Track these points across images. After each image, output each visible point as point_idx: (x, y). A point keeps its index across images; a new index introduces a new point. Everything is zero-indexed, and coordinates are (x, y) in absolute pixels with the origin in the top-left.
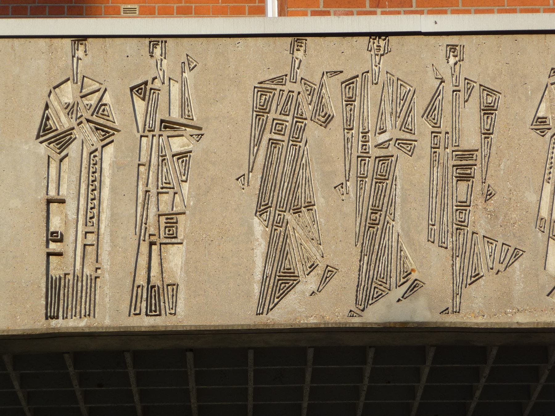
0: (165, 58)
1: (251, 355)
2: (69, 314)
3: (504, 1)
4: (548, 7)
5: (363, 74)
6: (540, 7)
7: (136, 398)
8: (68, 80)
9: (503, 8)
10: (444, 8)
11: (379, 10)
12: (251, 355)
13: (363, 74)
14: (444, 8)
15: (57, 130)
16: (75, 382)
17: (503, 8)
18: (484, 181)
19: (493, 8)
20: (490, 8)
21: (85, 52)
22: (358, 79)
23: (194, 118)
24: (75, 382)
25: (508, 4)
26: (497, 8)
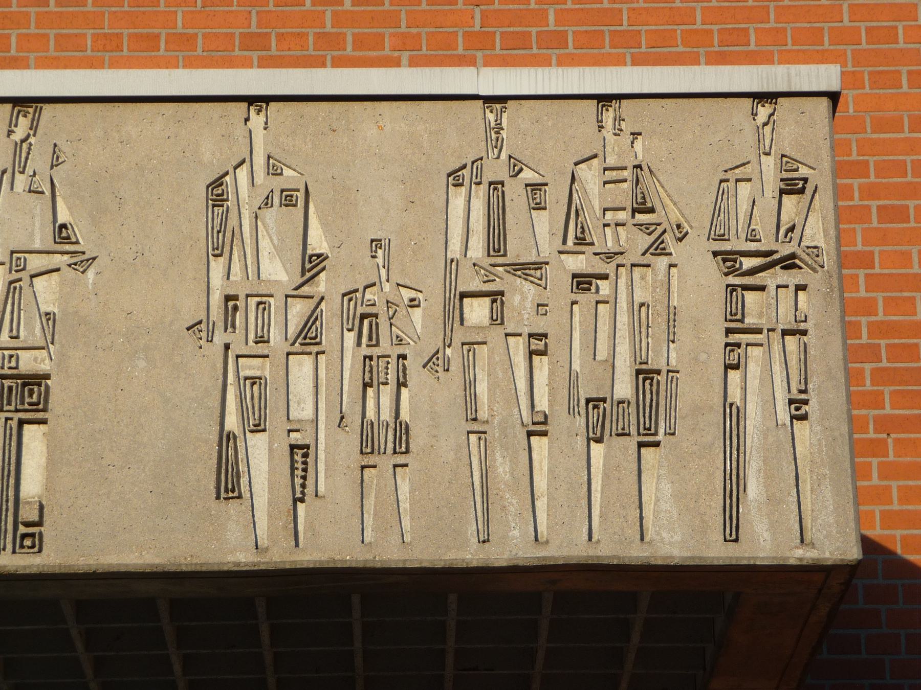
0: (34, 135)
1: (356, 599)
2: (607, 432)
3: (3, 12)
4: (174, 31)
5: (473, 163)
6: (160, 30)
7: (177, 668)
8: (595, 156)
9: (102, 31)
10: (6, 32)
11: (405, 56)
12: (356, 599)
13: (473, 163)
14: (6, 32)
15: (77, 243)
16: (79, 645)
17: (102, 31)
18: (671, 338)
19: (84, 31)
20: (79, 31)
21: (266, 123)
22: (464, 171)
23: (81, 241)
24: (79, 645)
25: (109, 25)
26: (92, 31)
